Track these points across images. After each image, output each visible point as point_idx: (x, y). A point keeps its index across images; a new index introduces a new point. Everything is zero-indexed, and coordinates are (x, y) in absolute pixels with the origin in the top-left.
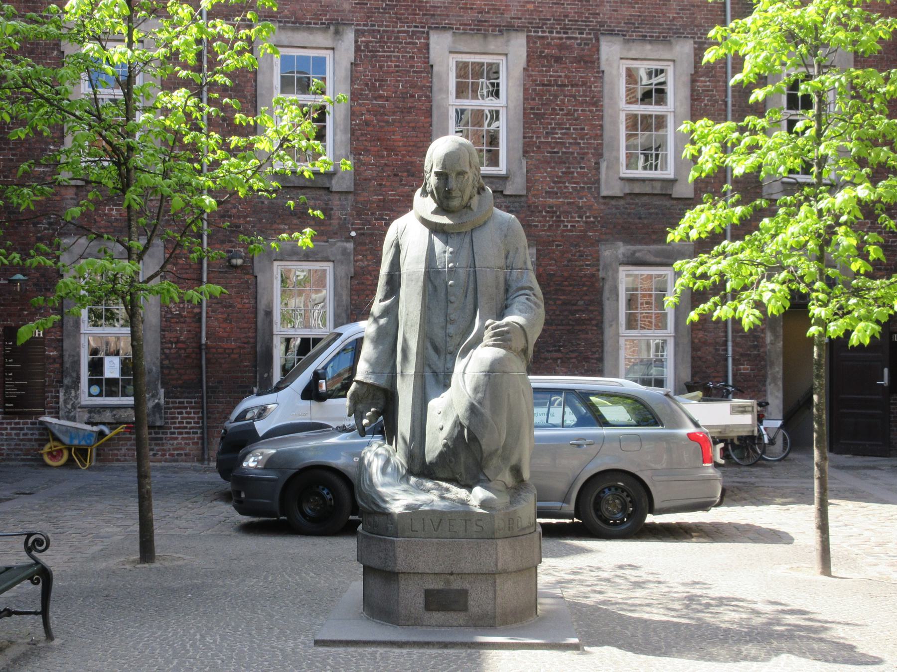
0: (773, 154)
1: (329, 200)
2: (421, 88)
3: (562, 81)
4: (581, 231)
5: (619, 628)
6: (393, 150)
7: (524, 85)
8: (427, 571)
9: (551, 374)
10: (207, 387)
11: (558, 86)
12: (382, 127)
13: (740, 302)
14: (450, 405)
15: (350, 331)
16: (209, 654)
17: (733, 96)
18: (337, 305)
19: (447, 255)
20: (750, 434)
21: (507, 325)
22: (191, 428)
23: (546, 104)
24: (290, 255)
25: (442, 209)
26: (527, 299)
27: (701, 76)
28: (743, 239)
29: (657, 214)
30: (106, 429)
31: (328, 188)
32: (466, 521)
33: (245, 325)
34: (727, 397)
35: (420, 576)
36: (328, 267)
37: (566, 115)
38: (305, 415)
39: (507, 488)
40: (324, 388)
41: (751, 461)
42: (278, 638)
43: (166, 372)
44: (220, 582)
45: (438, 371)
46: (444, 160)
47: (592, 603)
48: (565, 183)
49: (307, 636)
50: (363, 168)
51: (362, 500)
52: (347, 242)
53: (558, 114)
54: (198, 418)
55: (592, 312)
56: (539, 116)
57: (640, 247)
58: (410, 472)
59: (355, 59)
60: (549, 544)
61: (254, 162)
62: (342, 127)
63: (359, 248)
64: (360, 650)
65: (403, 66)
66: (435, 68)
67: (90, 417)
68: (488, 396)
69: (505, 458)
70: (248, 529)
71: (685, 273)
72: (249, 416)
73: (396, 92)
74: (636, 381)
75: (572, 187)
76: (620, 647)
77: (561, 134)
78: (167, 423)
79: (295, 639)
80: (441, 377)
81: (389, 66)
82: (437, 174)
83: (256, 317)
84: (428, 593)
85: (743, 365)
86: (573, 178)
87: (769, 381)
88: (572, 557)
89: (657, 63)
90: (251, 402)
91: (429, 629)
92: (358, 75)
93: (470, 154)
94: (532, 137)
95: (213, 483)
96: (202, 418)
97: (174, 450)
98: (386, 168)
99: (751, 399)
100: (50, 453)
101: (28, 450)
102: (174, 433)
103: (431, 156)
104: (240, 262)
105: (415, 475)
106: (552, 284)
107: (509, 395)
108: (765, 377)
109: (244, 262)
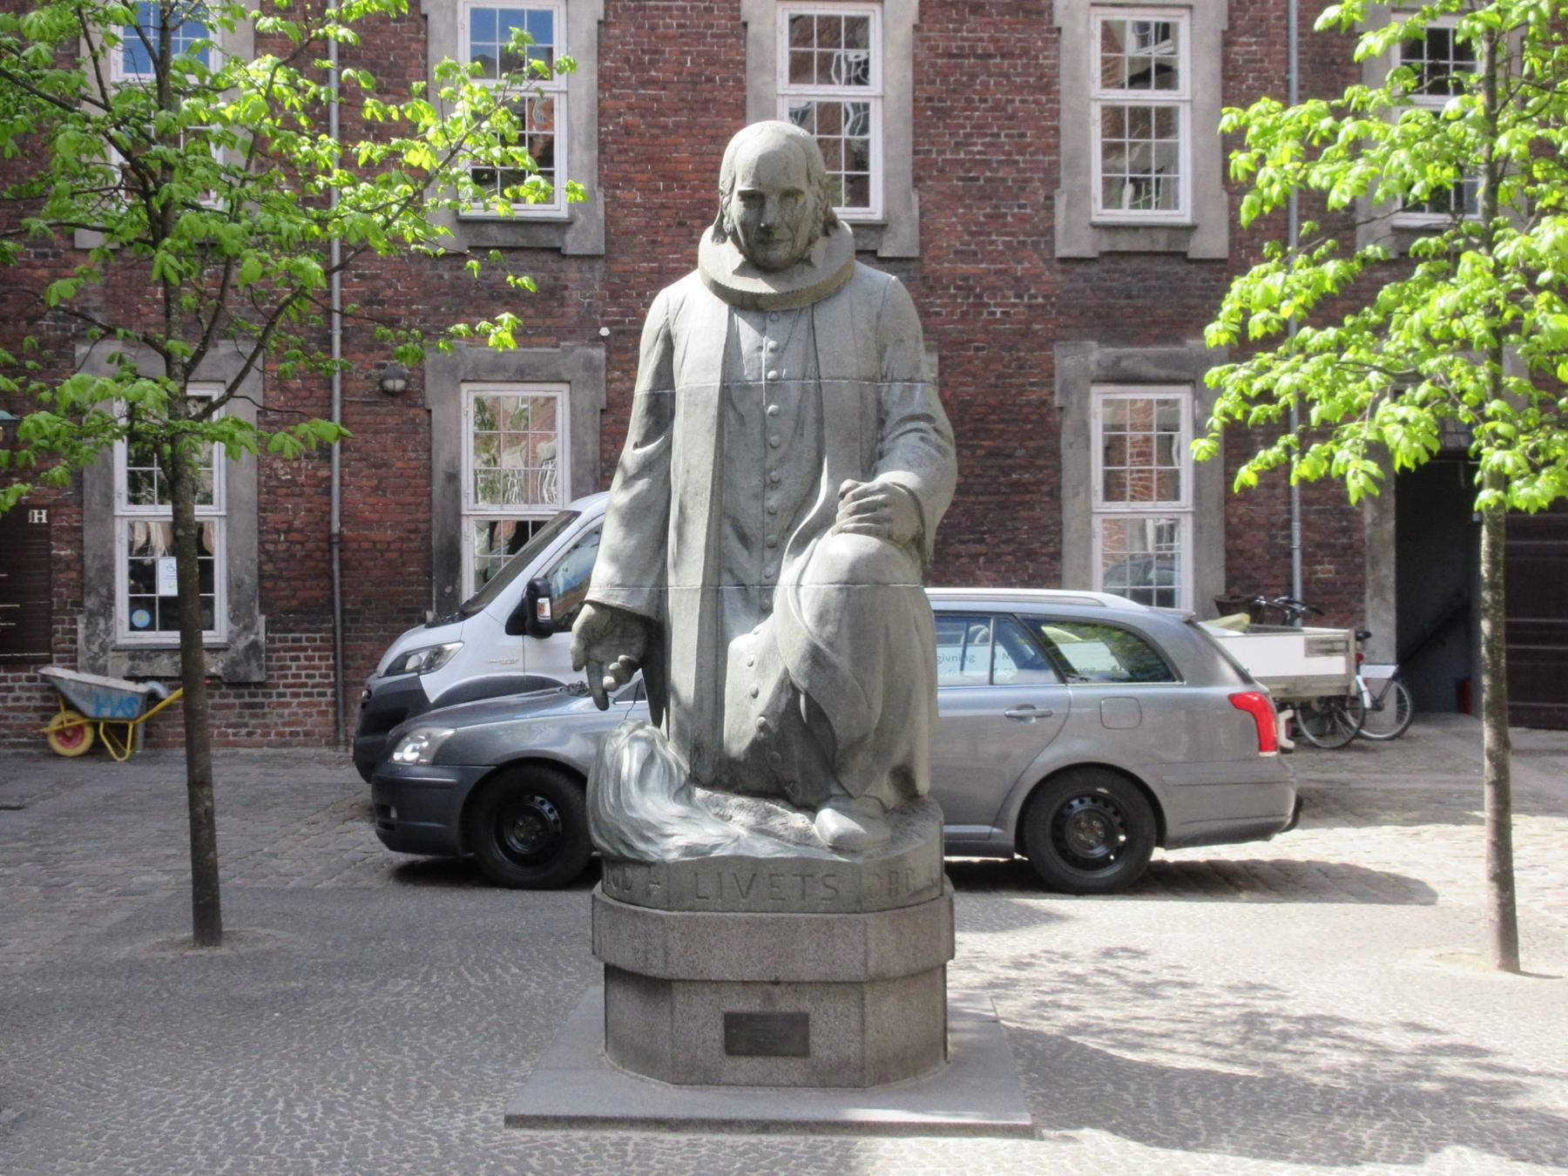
0: (1401, 155)
1: (562, 270)
2: (725, 65)
3: (984, 49)
4: (1020, 322)
5: (1109, 1088)
6: (675, 179)
7: (915, 56)
8: (729, 977)
9: (968, 585)
10: (343, 612)
11: (977, 57)
12: (655, 137)
13: (1338, 444)
14: (772, 650)
15: (592, 506)
16: (298, 1145)
17: (1301, 71)
18: (577, 462)
19: (763, 354)
20: (1343, 693)
21: (884, 489)
22: (314, 686)
23: (954, 91)
24: (492, 372)
25: (755, 264)
26: (922, 439)
27: (1240, 35)
28: (1340, 324)
29: (1160, 289)
30: (158, 687)
31: (558, 250)
32: (803, 877)
33: (412, 499)
34: (1291, 623)
35: (714, 987)
36: (561, 393)
37: (992, 109)
38: (512, 662)
39: (886, 810)
40: (547, 612)
41: (1340, 741)
42: (436, 1110)
43: (269, 584)
44: (339, 987)
45: (747, 582)
46: (758, 168)
47: (1055, 1031)
48: (989, 234)
49: (492, 1105)
50: (620, 212)
51: (602, 836)
52: (593, 346)
53: (977, 109)
54: (328, 667)
55: (1040, 469)
56: (941, 113)
57: (1127, 350)
58: (695, 779)
59: (606, 14)
60: (968, 903)
61: (404, 189)
62: (583, 138)
63: (615, 357)
64: (596, 1135)
65: (692, 26)
66: (752, 29)
67: (132, 668)
68: (845, 630)
69: (881, 753)
70: (407, 875)
71: (1229, 389)
72: (411, 664)
73: (680, 73)
74: (1122, 593)
75: (1004, 243)
76: (1114, 1130)
77: (983, 144)
78: (271, 677)
79: (469, 1112)
80: (754, 592)
81: (667, 27)
82: (744, 196)
83: (429, 484)
84: (733, 1022)
85: (1321, 563)
86: (1005, 225)
87: (1369, 592)
88: (1011, 933)
89: (1158, 11)
90: (416, 640)
91: (733, 1090)
92: (612, 42)
93: (809, 156)
94: (929, 152)
95: (344, 786)
96: (334, 668)
97: (285, 724)
98: (664, 212)
99: (1338, 625)
100: (60, 733)
101: (23, 727)
102: (282, 695)
103: (732, 162)
104: (399, 384)
105: (704, 786)
106: (967, 418)
107: (887, 627)
108: (1361, 586)
109: (408, 384)
